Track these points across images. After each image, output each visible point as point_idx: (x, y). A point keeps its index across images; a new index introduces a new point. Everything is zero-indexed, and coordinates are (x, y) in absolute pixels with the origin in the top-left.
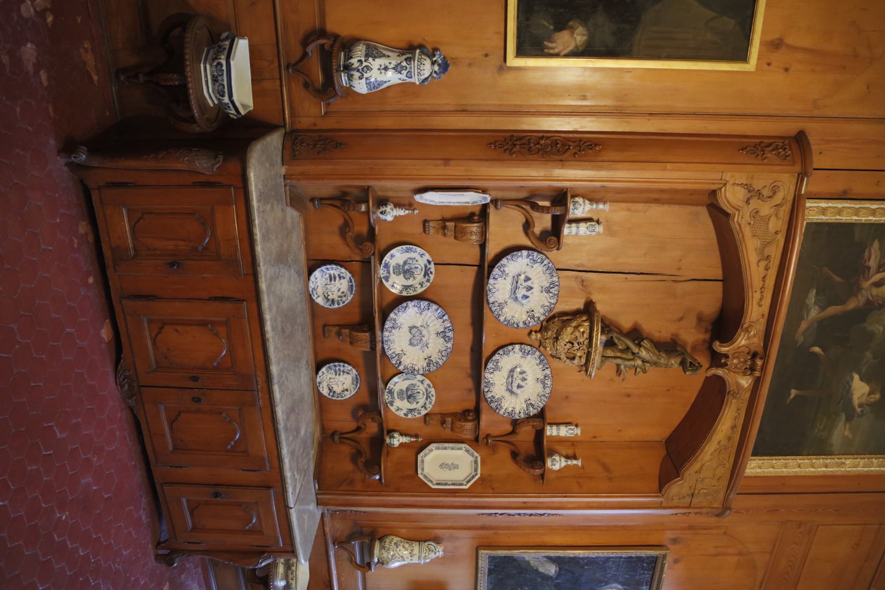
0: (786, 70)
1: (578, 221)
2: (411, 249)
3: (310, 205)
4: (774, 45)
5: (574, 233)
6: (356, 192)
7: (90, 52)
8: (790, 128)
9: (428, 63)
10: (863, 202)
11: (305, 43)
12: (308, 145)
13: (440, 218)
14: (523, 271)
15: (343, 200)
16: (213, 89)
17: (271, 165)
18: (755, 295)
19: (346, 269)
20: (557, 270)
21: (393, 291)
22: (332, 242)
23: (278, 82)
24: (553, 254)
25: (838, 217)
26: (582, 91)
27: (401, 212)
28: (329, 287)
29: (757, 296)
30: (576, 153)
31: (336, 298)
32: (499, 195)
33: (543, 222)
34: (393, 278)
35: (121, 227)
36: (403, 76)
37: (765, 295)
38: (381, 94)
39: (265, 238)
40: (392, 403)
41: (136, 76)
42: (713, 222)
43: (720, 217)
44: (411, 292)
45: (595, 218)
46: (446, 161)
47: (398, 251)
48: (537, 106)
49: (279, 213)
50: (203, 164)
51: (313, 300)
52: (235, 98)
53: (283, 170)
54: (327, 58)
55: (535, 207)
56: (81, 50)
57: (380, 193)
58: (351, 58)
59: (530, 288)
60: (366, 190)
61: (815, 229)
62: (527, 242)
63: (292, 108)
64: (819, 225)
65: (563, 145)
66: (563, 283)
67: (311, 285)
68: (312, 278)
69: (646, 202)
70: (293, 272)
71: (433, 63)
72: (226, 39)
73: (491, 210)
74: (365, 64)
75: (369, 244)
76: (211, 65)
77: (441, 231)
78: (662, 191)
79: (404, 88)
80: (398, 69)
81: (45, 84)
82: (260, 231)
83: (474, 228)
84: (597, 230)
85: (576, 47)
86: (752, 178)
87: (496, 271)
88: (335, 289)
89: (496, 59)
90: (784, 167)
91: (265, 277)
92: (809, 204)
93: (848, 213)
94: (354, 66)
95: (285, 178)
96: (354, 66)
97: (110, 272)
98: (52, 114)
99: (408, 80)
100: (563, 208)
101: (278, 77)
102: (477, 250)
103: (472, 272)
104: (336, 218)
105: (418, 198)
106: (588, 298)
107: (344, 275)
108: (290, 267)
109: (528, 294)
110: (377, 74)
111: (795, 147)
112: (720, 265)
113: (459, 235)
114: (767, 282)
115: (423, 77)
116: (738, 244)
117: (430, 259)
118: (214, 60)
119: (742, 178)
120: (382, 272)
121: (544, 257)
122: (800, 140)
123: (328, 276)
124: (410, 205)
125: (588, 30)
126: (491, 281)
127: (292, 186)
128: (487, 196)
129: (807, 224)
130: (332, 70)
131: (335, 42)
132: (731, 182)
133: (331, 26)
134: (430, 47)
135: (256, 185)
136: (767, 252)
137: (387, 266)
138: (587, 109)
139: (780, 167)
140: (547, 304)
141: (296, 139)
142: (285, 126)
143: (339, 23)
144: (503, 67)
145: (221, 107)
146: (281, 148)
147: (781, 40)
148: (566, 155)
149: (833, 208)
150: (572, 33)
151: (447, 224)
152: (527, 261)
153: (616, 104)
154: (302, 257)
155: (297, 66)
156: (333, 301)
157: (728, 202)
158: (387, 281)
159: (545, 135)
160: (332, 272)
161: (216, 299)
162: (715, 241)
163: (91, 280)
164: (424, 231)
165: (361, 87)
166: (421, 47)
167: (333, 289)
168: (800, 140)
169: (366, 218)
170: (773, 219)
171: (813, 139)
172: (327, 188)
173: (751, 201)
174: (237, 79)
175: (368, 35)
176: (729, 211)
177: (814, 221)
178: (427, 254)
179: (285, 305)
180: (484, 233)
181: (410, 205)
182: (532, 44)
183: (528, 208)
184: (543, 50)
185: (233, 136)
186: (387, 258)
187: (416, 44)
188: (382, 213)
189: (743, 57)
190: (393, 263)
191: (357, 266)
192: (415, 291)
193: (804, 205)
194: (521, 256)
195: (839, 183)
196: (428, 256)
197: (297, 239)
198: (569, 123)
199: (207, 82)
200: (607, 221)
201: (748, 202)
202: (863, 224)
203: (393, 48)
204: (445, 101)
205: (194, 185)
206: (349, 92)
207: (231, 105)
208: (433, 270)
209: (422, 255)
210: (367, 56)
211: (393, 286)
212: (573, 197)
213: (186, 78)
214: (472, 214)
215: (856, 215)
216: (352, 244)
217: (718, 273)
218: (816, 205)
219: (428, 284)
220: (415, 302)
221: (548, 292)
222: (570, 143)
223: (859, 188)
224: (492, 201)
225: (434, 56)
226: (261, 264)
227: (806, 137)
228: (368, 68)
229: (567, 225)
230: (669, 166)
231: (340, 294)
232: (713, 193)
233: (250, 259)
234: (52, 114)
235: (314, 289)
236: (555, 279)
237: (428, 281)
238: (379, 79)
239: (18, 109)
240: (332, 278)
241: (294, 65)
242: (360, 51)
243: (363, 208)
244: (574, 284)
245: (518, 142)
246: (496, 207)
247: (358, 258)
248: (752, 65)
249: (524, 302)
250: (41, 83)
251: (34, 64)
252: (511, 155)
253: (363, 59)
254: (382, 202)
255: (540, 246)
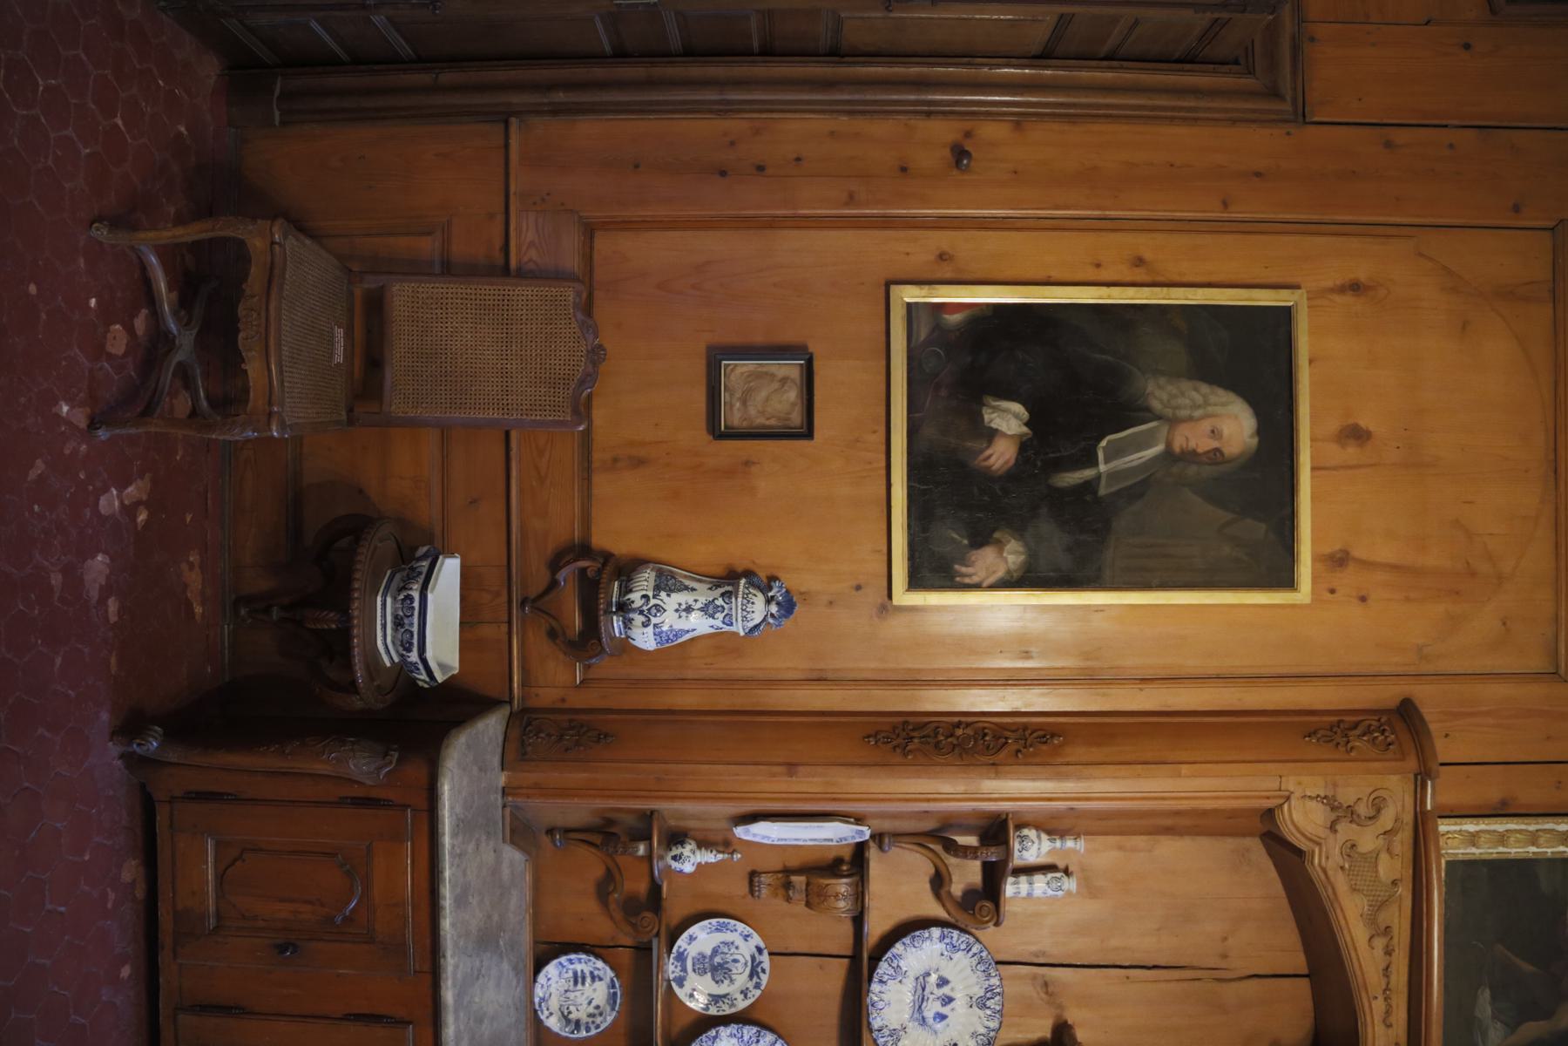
0: (1363, 599)
1: (1029, 870)
2: (725, 926)
3: (546, 840)
4: (1335, 561)
5: (1024, 893)
6: (630, 820)
7: (197, 569)
8: (1387, 694)
9: (759, 600)
10: (1540, 820)
11: (555, 564)
12: (549, 735)
13: (779, 867)
14: (934, 966)
15: (606, 834)
16: (394, 638)
17: (481, 769)
18: (1374, 1003)
19: (605, 961)
20: (998, 963)
21: (692, 1005)
22: (580, 908)
23: (504, 628)
24: (989, 933)
25: (1501, 849)
26: (1022, 645)
27: (710, 857)
28: (571, 995)
29: (1379, 1006)
30: (1018, 751)
31: (584, 1019)
32: (887, 825)
33: (966, 874)
34: (693, 980)
35: (200, 870)
36: (718, 623)
37: (1394, 1004)
38: (678, 650)
39: (460, 901)
40: (681, 982)
41: (267, 610)
42: (1276, 866)
43: (1288, 858)
44: (725, 1007)
45: (1061, 865)
46: (791, 767)
47: (703, 929)
48: (948, 670)
49: (488, 857)
50: (362, 766)
51: (540, 1021)
52: (429, 655)
53: (502, 779)
54: (590, 591)
55: (951, 847)
56: (184, 566)
57: (672, 823)
58: (631, 591)
59: (948, 1000)
60: (648, 817)
61: (1465, 873)
62: (938, 911)
63: (525, 670)
64: (1471, 864)
65: (996, 738)
66: (1010, 989)
67: (539, 992)
68: (541, 978)
69: (1150, 834)
70: (506, 966)
71: (769, 601)
72: (424, 557)
73: (873, 853)
74: (653, 602)
75: (648, 915)
76: (394, 599)
77: (781, 892)
78: (1178, 813)
79: (720, 643)
80: (708, 610)
81: (113, 618)
82: (452, 891)
83: (842, 886)
84: (1066, 887)
85: (1009, 572)
86: (1335, 785)
87: (883, 968)
88: (583, 1000)
89: (874, 594)
90: (1387, 764)
91: (454, 978)
92: (1444, 827)
93: (1518, 841)
94: (634, 606)
95: (504, 792)
96: (634, 606)
97: (164, 957)
98: (114, 669)
99: (726, 628)
100: (1001, 849)
101: (506, 618)
102: (847, 928)
103: (839, 969)
104: (591, 864)
105: (740, 832)
106: (1058, 1017)
107: (601, 973)
108: (501, 956)
109: (945, 1010)
110: (673, 618)
111: (1399, 728)
112: (1299, 946)
113: (815, 898)
114: (1393, 978)
115: (751, 624)
116: (1327, 905)
117: (762, 945)
118: (400, 590)
119: (1313, 783)
120: (671, 968)
121: (972, 940)
122: (1407, 712)
123: (571, 974)
124: (726, 845)
125: (1026, 545)
126: (875, 987)
127: (517, 808)
128: (865, 829)
129: (1448, 863)
130: (597, 610)
131: (604, 565)
132: (1298, 793)
133: (599, 540)
134: (763, 575)
135: (452, 808)
136: (1384, 918)
137: (681, 957)
138: (1033, 675)
139: (1377, 765)
140: (983, 1030)
141: (529, 724)
142: (510, 702)
143: (616, 532)
144: (886, 606)
145: (403, 668)
146: (501, 739)
147: (1347, 553)
148: (1002, 755)
149: (1488, 832)
150: (1001, 551)
151: (794, 878)
152: (939, 947)
153: (1082, 664)
154: (526, 938)
155: (539, 603)
156: (578, 1023)
157: (1303, 835)
158: (681, 985)
159: (963, 719)
160: (579, 967)
161: (358, 1017)
162: (1285, 902)
163: (126, 972)
164: (752, 892)
165: (645, 639)
166: (748, 574)
167: (579, 1001)
168: (1407, 712)
169: (644, 867)
170: (1384, 857)
171: (1428, 712)
172: (578, 811)
173: (1338, 827)
174: (436, 624)
175: (663, 556)
176: (1303, 848)
177: (1461, 857)
178: (755, 935)
179: (486, 1029)
180: (860, 895)
181: (726, 844)
182: (931, 570)
183: (938, 848)
184: (952, 578)
185: (423, 717)
186: (682, 942)
187: (740, 570)
188: (674, 858)
189: (1284, 578)
190: (692, 951)
191: (625, 956)
192: (732, 1005)
193: (1437, 835)
194: (930, 938)
195: (1491, 789)
196: (756, 940)
197: (518, 902)
198: (1003, 699)
199: (384, 626)
200: (1083, 870)
201: (1332, 827)
202: (1549, 860)
203: (701, 576)
204: (784, 660)
205: (342, 802)
206: (625, 646)
207: (421, 666)
208: (766, 965)
209: (746, 937)
210: (658, 588)
211: (692, 996)
212: (1019, 827)
213: (349, 618)
214: (839, 861)
215: (1533, 844)
216: (618, 915)
217: (1299, 962)
218: (1457, 828)
219: (758, 993)
220: (733, 1028)
221: (983, 1006)
222: (1008, 734)
223: (1529, 795)
224: (872, 836)
225: (770, 589)
226: (449, 953)
227: (1416, 709)
228: (659, 609)
229: (1010, 880)
230: (1185, 769)
231: (591, 1010)
232: (1269, 814)
233: (428, 941)
234: (114, 669)
235: (543, 999)
236: (995, 981)
237: (757, 986)
238: (676, 627)
239: (58, 661)
240: (578, 979)
241: (534, 600)
242: (645, 581)
243: (642, 849)
244: (1032, 991)
245: (915, 734)
246: (881, 847)
247: (628, 941)
248: (1304, 591)
249: (939, 1026)
250: (107, 619)
251: (101, 587)
252: (905, 755)
253: (650, 594)
254: (676, 838)
255: (962, 918)
